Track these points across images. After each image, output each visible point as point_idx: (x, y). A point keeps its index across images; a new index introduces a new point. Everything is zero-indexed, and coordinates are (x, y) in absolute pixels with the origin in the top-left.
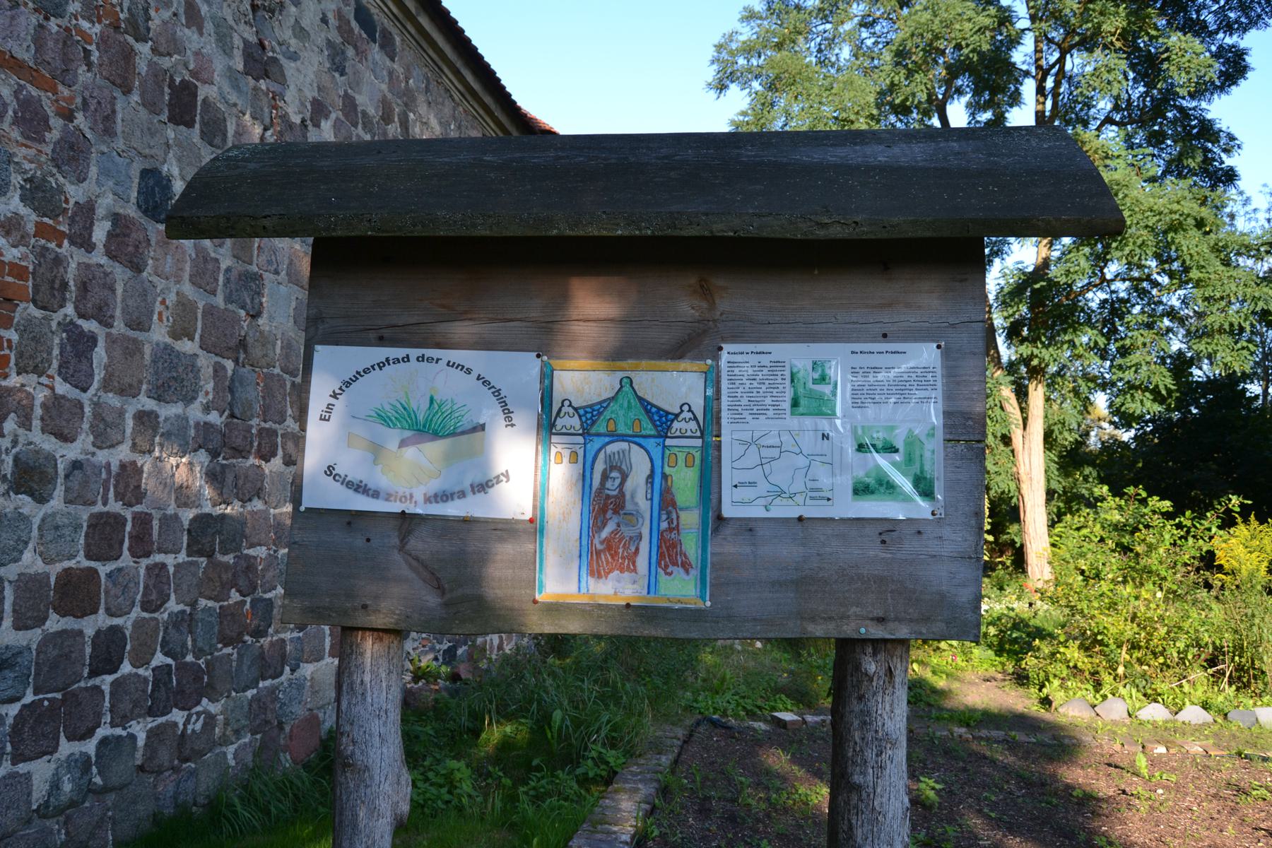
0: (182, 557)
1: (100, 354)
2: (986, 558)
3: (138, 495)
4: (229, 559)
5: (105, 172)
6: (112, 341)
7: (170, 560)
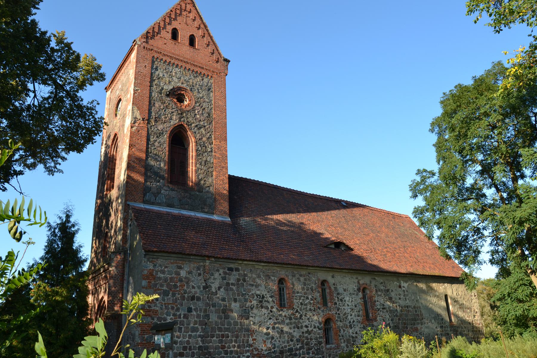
0: (197, 351)
1: (183, 329)
2: (74, 296)
3: (189, 344)
4: (206, 351)
5: (182, 310)
7: (195, 351)
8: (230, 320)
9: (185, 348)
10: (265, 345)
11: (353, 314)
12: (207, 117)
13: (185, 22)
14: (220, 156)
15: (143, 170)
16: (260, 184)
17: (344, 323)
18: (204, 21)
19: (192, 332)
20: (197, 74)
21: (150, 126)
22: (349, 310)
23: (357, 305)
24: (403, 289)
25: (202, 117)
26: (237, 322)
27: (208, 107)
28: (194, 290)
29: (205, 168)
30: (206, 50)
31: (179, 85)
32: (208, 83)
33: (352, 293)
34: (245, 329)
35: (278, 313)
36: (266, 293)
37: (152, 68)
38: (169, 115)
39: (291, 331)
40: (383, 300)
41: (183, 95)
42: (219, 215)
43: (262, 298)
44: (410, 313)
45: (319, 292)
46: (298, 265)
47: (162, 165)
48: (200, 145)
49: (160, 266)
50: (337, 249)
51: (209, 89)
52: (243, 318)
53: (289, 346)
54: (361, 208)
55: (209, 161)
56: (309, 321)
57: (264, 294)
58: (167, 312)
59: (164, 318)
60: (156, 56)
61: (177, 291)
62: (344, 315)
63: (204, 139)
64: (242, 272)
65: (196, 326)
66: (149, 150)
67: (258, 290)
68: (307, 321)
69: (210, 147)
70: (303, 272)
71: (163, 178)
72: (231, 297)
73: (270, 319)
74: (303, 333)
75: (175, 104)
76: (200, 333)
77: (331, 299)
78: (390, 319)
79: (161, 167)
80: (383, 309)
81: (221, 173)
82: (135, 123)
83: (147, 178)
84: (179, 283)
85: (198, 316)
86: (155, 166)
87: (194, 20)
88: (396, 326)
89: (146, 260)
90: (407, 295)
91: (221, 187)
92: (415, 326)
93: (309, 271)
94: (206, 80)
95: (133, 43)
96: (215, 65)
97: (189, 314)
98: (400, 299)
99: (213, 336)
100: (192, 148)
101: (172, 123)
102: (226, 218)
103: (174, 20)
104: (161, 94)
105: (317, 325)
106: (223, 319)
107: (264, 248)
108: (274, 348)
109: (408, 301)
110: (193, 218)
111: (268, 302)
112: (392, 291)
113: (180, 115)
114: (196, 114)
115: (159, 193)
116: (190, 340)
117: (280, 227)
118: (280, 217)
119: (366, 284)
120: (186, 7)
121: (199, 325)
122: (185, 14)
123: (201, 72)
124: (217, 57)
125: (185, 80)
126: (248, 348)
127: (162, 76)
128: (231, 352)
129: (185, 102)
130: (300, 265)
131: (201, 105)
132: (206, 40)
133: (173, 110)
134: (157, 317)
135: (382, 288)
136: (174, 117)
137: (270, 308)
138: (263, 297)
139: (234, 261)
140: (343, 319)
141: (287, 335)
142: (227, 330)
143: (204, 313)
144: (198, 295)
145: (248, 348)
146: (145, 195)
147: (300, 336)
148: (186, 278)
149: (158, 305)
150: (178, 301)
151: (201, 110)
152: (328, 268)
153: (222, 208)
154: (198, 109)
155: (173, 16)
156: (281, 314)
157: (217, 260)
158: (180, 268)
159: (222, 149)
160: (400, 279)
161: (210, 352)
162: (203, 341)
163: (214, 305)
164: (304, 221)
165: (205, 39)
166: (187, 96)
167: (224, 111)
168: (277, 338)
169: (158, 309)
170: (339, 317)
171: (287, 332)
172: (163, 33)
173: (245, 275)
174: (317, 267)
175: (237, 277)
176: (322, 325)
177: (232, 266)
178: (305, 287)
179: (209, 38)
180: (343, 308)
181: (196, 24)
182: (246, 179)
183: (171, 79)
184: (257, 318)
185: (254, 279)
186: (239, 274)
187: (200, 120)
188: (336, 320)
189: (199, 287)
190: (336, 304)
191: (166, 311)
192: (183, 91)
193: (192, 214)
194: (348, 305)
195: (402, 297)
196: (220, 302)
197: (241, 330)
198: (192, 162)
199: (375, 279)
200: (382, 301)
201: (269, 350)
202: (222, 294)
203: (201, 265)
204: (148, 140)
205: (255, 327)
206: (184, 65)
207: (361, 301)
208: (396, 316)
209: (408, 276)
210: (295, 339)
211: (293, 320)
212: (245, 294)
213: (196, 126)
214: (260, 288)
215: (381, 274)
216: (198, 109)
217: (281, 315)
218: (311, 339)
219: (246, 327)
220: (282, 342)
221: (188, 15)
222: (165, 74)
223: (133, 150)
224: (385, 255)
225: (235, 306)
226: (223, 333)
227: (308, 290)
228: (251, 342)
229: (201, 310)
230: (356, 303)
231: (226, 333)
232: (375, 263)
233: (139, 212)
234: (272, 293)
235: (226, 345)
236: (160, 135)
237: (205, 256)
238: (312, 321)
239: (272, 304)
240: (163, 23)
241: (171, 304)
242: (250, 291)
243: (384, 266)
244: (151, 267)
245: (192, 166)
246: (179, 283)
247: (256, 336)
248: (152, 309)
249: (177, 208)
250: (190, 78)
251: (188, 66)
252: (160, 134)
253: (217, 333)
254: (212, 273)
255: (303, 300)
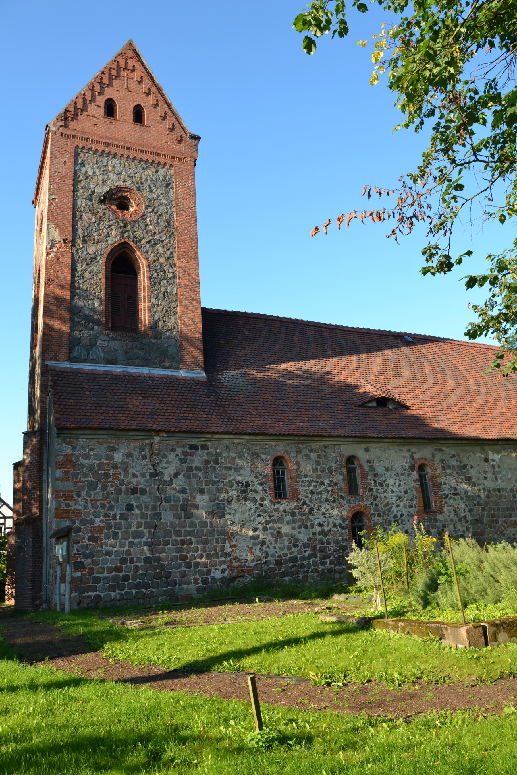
0: (143, 564)
1: (120, 534)
3: (130, 554)
4: (156, 564)
6: (122, 532)
7: (139, 564)
8: (194, 519)
9: (123, 561)
10: (252, 553)
11: (402, 504)
12: (166, 226)
13: (125, 87)
14: (187, 284)
15: (66, 314)
16: (267, 320)
17: (385, 518)
18: (157, 81)
19: (134, 538)
20: (147, 164)
21: (75, 249)
22: (394, 499)
23: (409, 491)
24: (492, 463)
25: (157, 228)
26: (206, 522)
27: (167, 212)
28: (135, 479)
29: (164, 303)
30: (161, 126)
31: (120, 183)
32: (165, 177)
33: (400, 473)
34: (218, 531)
35: (273, 507)
36: (253, 478)
37: (75, 163)
38: (105, 231)
39: (296, 532)
40: (454, 481)
41: (126, 198)
42: (188, 369)
43: (246, 486)
44: (504, 500)
45: (342, 474)
46: (305, 435)
47: (97, 305)
48: (156, 270)
49: (83, 448)
50: (380, 408)
51: (168, 185)
52: (215, 516)
53: (290, 554)
54: (439, 344)
55: (170, 293)
56: (325, 517)
57: (250, 480)
58: (95, 512)
59: (91, 519)
60: (80, 145)
61: (110, 482)
62: (386, 506)
63: (162, 260)
64: (213, 451)
65: (140, 529)
66: (76, 284)
67: (240, 475)
68: (322, 517)
69: (171, 271)
70: (315, 446)
71: (99, 324)
72: (196, 486)
73: (259, 515)
74: (314, 534)
75: (114, 213)
76: (147, 539)
77: (363, 484)
78: (467, 510)
79: (95, 308)
80: (455, 494)
81: (190, 308)
82: (51, 248)
83: (73, 325)
84: (112, 470)
85: (143, 516)
86: (85, 306)
87: (140, 82)
88: (477, 520)
89: (60, 441)
90: (500, 473)
91: (190, 328)
92: (512, 519)
93: (326, 444)
94: (162, 171)
95: (46, 129)
96: (177, 147)
97: (129, 513)
98: (485, 478)
99: (167, 543)
100: (144, 275)
101: (110, 242)
102: (199, 374)
103: (108, 86)
104: (91, 200)
105: (339, 521)
106: (183, 519)
107: (254, 413)
108: (266, 557)
109: (500, 481)
110: (144, 377)
111: (256, 491)
112: (472, 467)
113: (122, 229)
114: (148, 225)
115: (93, 345)
116: (132, 549)
117: (288, 381)
118: (292, 366)
119: (426, 459)
120: (126, 63)
121: (145, 528)
122: (125, 75)
123: (153, 161)
124: (179, 135)
125: (129, 176)
126: (223, 559)
127: (91, 174)
128: (197, 565)
129: (130, 208)
130: (309, 436)
131: (155, 211)
132: (162, 108)
133: (111, 222)
134: (80, 519)
135: (454, 463)
136: (113, 233)
137: (259, 500)
138: (248, 485)
139: (199, 436)
140: (384, 512)
141: (287, 538)
142: (188, 533)
143: (152, 511)
144: (141, 486)
145: (223, 559)
146: (71, 350)
147: (310, 539)
148: (123, 463)
149: (81, 503)
150: (112, 496)
151: (156, 217)
152: (356, 437)
153: (193, 360)
154: (151, 217)
155: (106, 81)
156: (277, 509)
157: (170, 435)
158: (114, 449)
159: (191, 272)
160: (486, 448)
161: (162, 565)
162: (151, 551)
163: (168, 500)
164: (332, 369)
165: (159, 108)
166: (132, 198)
167: (193, 215)
168: (271, 543)
169: (80, 508)
170: (377, 510)
171: (287, 535)
172: (91, 109)
173: (218, 454)
174: (337, 436)
175: (205, 457)
176: (347, 523)
177: (196, 442)
178: (319, 467)
179: (166, 106)
180: (383, 496)
181: (144, 87)
182: (245, 313)
183: (106, 177)
184: (237, 515)
185: (233, 459)
186: (207, 453)
187: (155, 233)
188: (372, 514)
189: (143, 475)
190: (371, 490)
191: (93, 511)
192: (127, 192)
193: (145, 371)
194: (393, 492)
195: (489, 475)
196: (178, 494)
197: (212, 532)
198: (144, 296)
199: (441, 450)
200: (453, 483)
201: (258, 561)
202: (181, 484)
203: (147, 444)
204: (73, 269)
205: (236, 528)
206: (126, 152)
207: (417, 485)
208: (479, 504)
209: (500, 443)
210: (301, 544)
211: (298, 517)
212: (218, 482)
213: (149, 242)
214: (242, 471)
215: (451, 442)
216: (151, 217)
217: (277, 510)
218: (329, 543)
219: (219, 528)
220: (279, 548)
221: (131, 75)
222: (97, 171)
223: (51, 286)
224: (466, 414)
225: (202, 500)
226: (183, 538)
227: (323, 472)
228: (228, 549)
229: (147, 507)
230: (406, 488)
231: (188, 538)
232: (444, 426)
233: (62, 374)
234: (263, 478)
235: (189, 555)
236: (92, 261)
237: (150, 430)
238: (330, 517)
239: (262, 494)
240: (90, 94)
241: (100, 500)
242: (225, 476)
243: (458, 430)
244: (69, 451)
245: (145, 302)
246: (112, 470)
247: (236, 541)
248: (72, 508)
249: (122, 365)
250: (136, 171)
251: (132, 154)
252: (93, 260)
253: (174, 538)
254: (164, 454)
255: (315, 486)
